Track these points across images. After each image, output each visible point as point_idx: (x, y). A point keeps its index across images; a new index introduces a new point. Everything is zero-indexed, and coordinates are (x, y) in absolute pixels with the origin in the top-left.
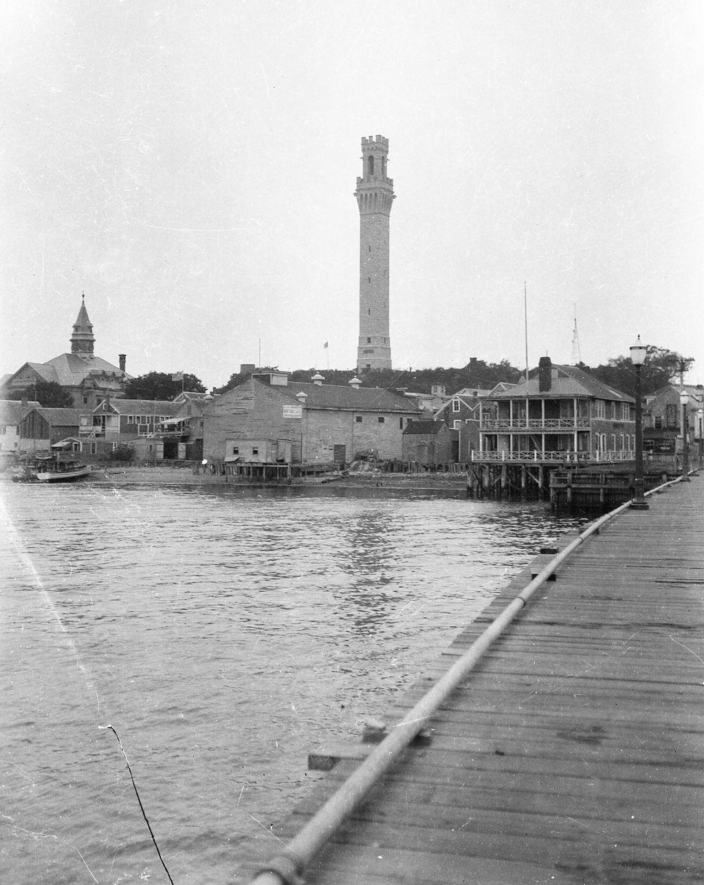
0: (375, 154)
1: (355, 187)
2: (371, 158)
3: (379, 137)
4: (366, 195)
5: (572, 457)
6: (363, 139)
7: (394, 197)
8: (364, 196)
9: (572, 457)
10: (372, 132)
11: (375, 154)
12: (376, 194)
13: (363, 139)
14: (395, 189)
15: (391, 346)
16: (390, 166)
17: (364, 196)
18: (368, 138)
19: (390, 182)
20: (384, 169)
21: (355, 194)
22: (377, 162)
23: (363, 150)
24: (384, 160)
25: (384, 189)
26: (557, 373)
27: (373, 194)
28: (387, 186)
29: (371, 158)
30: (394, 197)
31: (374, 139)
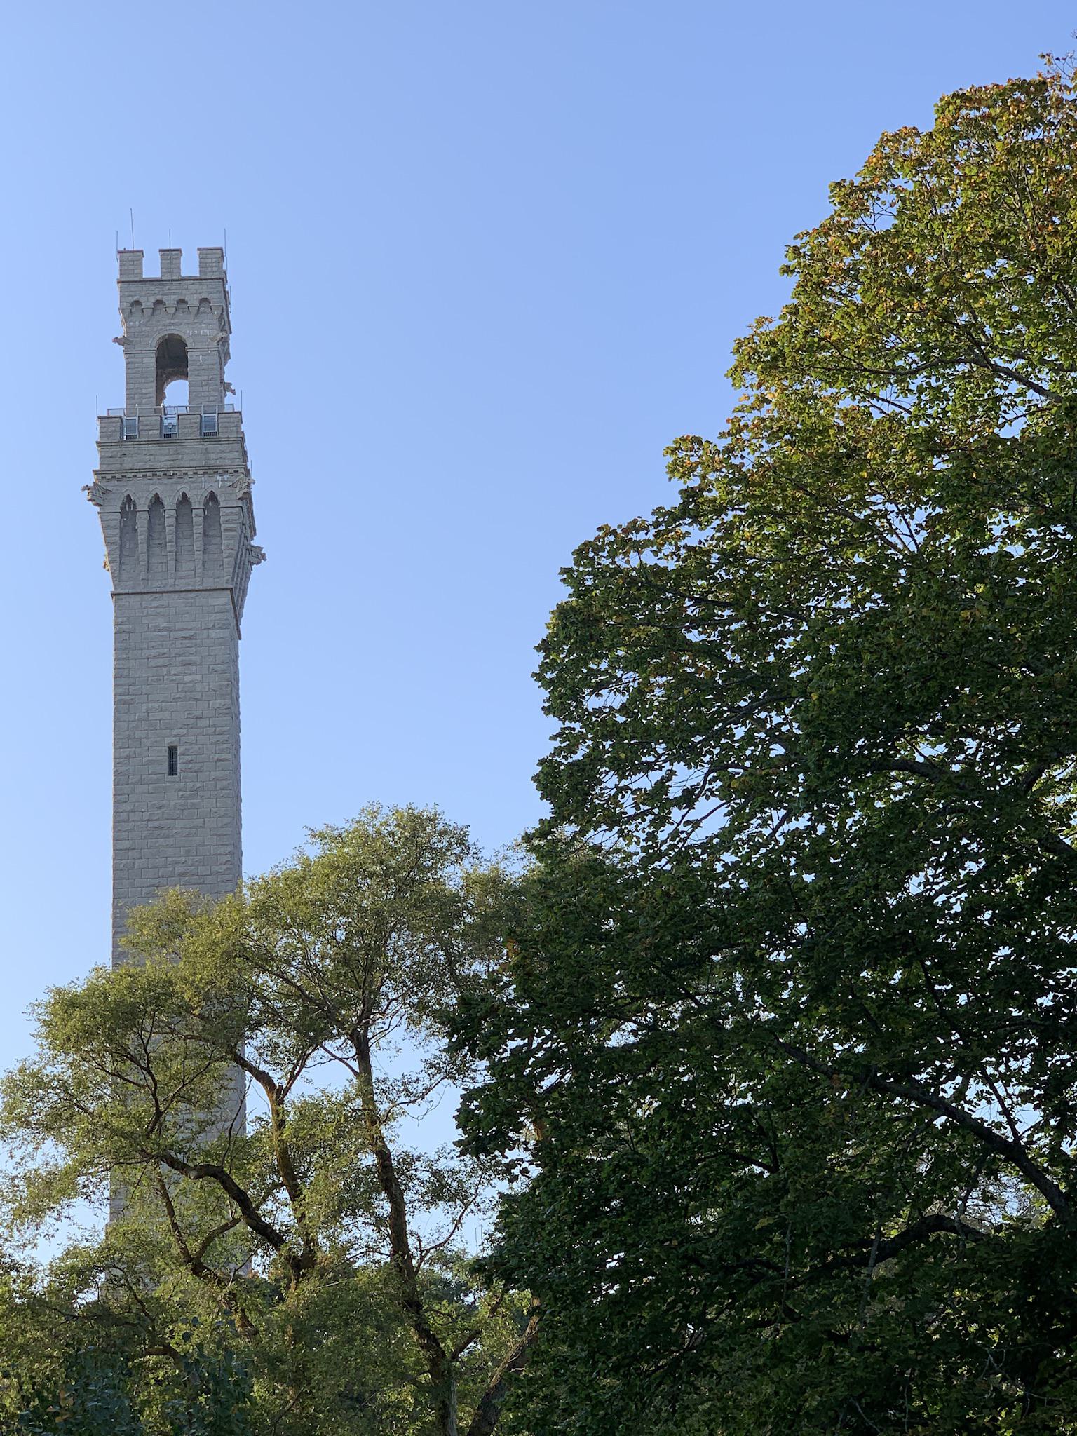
10: (173, 228)
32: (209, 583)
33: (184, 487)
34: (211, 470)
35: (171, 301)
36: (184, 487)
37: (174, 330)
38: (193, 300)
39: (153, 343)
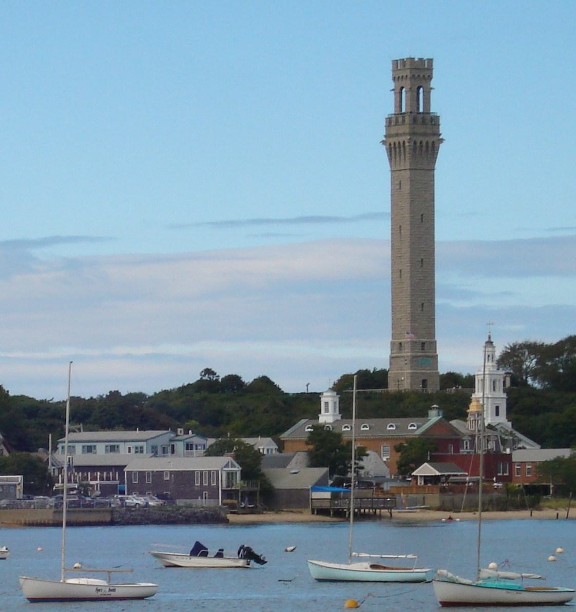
4: (421, 142)
17: (430, 145)
27: (424, 144)
35: (422, 75)
36: (427, 139)
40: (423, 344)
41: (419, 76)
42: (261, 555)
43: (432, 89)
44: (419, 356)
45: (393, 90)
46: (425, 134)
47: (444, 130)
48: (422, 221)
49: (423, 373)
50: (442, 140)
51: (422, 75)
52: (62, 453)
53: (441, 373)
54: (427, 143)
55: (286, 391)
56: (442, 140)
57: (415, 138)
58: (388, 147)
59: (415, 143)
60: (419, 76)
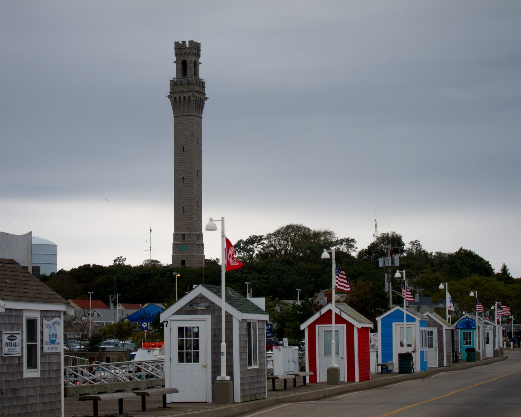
0: (187, 56)
1: (168, 89)
2: (184, 63)
3: (191, 42)
4: (180, 98)
5: (393, 262)
6: (177, 43)
7: (206, 98)
8: (187, 99)
9: (393, 262)
10: (186, 38)
11: (187, 56)
12: (189, 97)
13: (177, 43)
14: (206, 91)
15: (204, 242)
16: (202, 69)
17: (187, 99)
18: (181, 43)
19: (202, 84)
20: (196, 72)
21: (169, 97)
22: (190, 67)
23: (176, 54)
24: (196, 64)
25: (196, 92)
26: (60, 330)
27: (182, 98)
28: (198, 89)
29: (184, 63)
30: (206, 98)
31: (187, 44)
32: (189, 114)
33: (185, 95)
34: (189, 91)
35: (183, 52)
36: (185, 95)
37: (184, 59)
38: (187, 53)
39: (180, 62)
40: (184, 235)
41: (181, 53)
42: (175, 391)
43: (200, 63)
44: (179, 244)
45: (175, 62)
46: (181, 92)
47: (167, 89)
48: (184, 151)
49: (182, 256)
50: (206, 98)
51: (183, 52)
52: (488, 334)
53: (207, 257)
54: (185, 97)
55: (107, 265)
56: (206, 98)
57: (176, 95)
58: (173, 99)
59: (175, 98)
60: (181, 53)
